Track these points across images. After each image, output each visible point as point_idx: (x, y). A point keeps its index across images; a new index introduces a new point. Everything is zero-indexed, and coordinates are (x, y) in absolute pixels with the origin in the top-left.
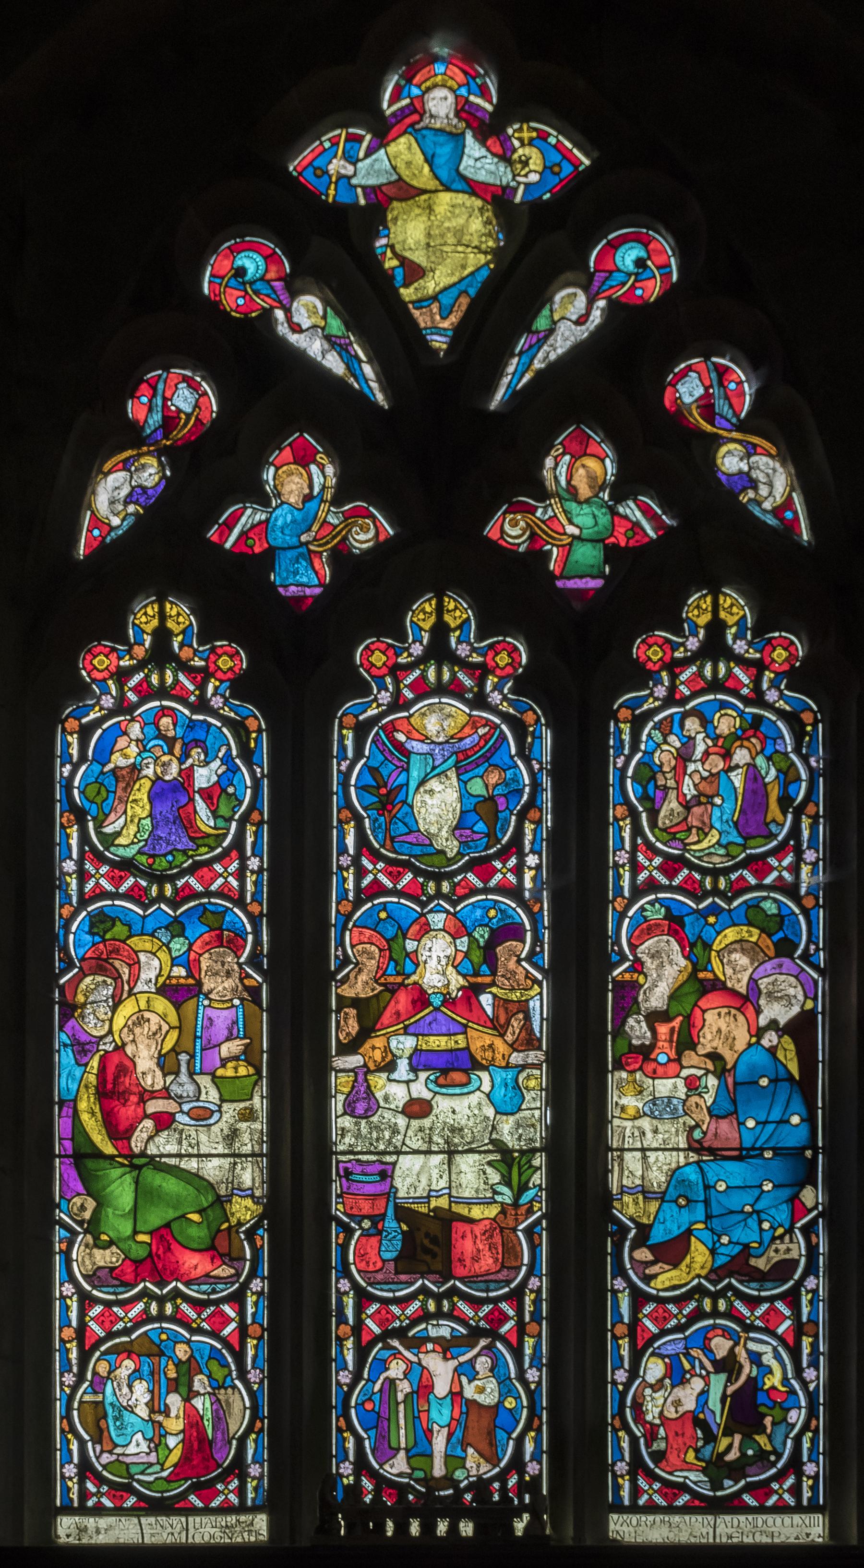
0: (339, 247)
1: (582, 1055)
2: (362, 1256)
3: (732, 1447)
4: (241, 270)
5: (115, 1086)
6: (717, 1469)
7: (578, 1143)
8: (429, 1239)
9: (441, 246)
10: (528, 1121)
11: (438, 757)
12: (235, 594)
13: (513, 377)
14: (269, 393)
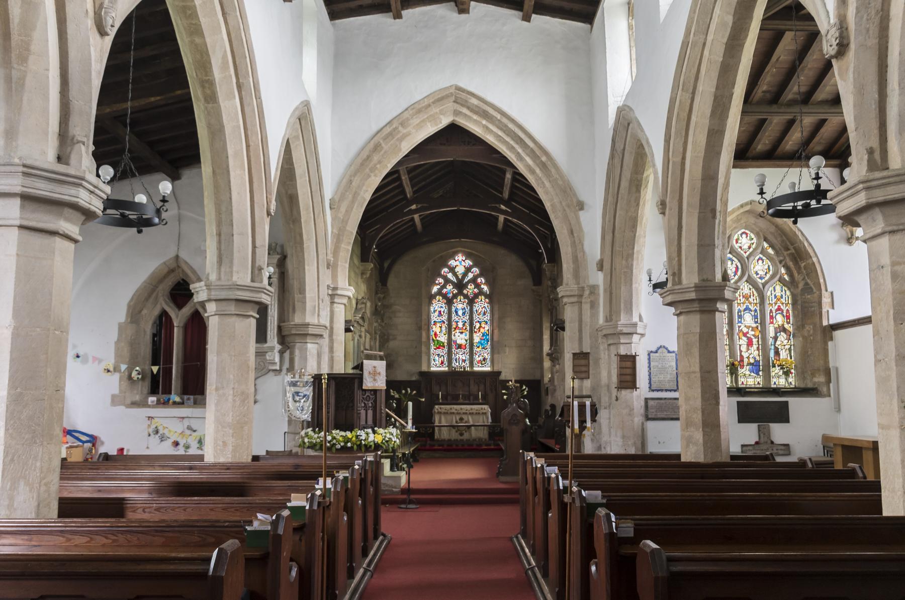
0: (452, 270)
1: (471, 332)
5: (436, 334)
7: (471, 338)
8: (460, 346)
9: (460, 270)
10: (467, 337)
11: (460, 305)
12: (444, 296)
13: (466, 280)
14: (447, 281)
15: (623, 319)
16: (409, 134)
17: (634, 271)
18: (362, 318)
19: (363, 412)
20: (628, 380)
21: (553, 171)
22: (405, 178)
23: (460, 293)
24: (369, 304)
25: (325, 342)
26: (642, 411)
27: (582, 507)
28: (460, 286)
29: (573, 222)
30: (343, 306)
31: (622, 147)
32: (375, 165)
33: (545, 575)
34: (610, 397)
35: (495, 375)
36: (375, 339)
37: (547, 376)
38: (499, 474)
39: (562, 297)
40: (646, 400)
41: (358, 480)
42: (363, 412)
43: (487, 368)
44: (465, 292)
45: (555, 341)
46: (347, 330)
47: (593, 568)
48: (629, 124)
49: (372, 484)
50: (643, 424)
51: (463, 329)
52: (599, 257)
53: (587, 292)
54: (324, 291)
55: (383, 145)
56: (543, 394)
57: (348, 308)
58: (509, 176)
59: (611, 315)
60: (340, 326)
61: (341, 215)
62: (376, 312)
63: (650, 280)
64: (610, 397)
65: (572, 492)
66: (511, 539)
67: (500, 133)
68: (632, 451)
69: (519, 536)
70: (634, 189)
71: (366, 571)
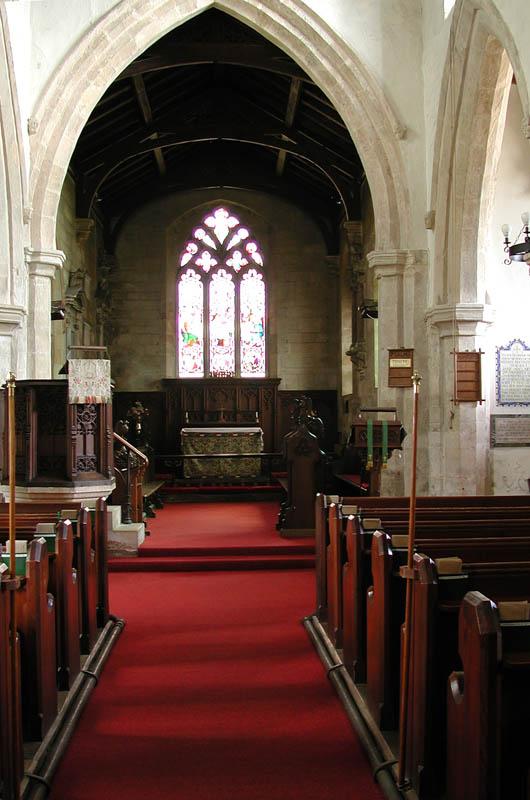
0: (210, 231)
2: (213, 345)
3: (255, 366)
4: (200, 234)
6: (253, 368)
11: (222, 283)
12: (199, 270)
14: (202, 247)
15: (464, 301)
16: (148, 22)
17: (480, 229)
18: (78, 300)
19: (79, 438)
20: (471, 392)
21: (362, 80)
22: (141, 91)
23: (222, 264)
24: (88, 280)
25: (22, 334)
26: (487, 433)
27: (430, 586)
28: (222, 254)
29: (391, 156)
30: (48, 280)
31: (465, 46)
32: (97, 68)
33: (360, 678)
34: (442, 415)
35: (271, 382)
36: (98, 332)
37: (347, 389)
38: (278, 527)
39: (375, 266)
40: (492, 417)
41: (71, 543)
42: (79, 438)
43: (261, 374)
44: (229, 263)
45: (361, 334)
46: (55, 316)
47: (454, 686)
48: (475, 10)
49: (93, 547)
50: (487, 452)
51: (222, 316)
52: (428, 210)
53: (411, 260)
54: (20, 259)
55: (109, 38)
56: (341, 409)
57: (57, 284)
58: (295, 90)
59: (445, 295)
60: (44, 309)
61: (44, 144)
62: (99, 293)
63: (507, 243)
64: (442, 415)
65: (413, 563)
66: (303, 624)
67: (283, 23)
68: (472, 492)
69: (315, 618)
70: (481, 108)
71: (87, 676)
